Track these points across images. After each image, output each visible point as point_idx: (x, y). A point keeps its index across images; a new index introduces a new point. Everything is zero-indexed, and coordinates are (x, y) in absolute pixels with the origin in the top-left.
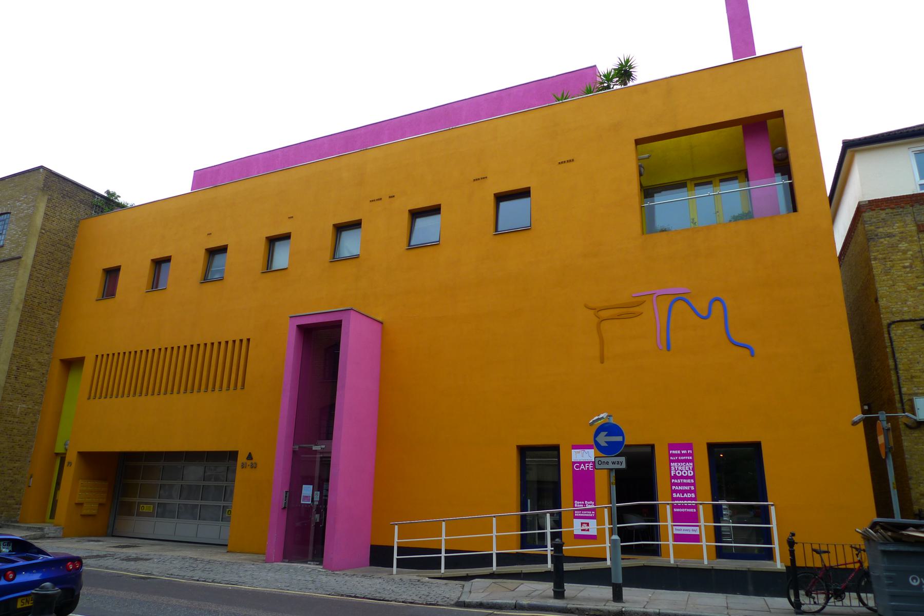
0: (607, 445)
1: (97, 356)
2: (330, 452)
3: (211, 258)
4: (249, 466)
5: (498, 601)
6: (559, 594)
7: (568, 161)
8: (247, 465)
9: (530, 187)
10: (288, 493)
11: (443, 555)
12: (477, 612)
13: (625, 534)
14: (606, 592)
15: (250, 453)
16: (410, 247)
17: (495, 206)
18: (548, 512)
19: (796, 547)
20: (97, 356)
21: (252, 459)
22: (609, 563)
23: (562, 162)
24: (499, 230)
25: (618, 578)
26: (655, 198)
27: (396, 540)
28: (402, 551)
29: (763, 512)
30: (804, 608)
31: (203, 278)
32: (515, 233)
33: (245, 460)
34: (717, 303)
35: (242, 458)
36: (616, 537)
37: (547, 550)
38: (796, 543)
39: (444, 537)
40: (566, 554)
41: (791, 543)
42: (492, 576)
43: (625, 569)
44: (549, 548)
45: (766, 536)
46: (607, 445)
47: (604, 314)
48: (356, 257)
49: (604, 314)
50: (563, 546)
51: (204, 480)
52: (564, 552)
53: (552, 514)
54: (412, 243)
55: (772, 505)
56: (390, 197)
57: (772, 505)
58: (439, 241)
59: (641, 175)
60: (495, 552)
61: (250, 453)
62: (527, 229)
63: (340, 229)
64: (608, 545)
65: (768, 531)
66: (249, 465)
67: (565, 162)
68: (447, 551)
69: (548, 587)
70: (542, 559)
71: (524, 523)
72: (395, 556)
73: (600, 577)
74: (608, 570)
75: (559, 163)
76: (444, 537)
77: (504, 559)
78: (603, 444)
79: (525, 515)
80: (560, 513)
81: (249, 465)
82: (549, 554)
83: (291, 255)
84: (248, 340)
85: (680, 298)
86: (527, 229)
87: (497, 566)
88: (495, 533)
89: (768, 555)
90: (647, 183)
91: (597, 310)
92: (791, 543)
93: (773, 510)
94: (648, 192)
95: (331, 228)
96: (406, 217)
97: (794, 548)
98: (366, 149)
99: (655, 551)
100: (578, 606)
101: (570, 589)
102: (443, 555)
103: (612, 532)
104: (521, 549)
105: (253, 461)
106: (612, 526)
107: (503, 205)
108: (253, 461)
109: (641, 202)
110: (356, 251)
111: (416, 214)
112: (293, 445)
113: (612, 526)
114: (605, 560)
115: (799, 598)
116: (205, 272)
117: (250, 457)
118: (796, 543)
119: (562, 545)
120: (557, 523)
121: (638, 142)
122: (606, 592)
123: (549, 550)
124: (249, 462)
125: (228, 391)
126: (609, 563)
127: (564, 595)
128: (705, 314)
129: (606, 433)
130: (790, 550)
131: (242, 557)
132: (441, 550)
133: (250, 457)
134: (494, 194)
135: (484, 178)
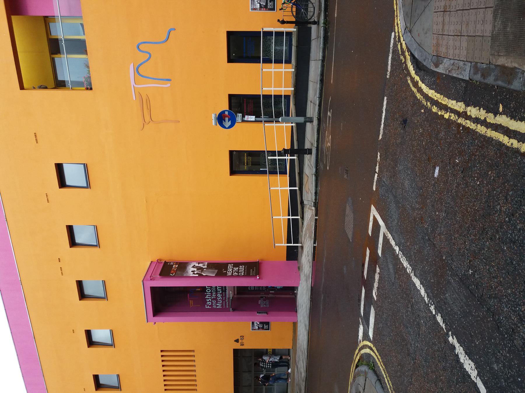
0: (230, 121)
1: (165, 390)
2: (234, 287)
3: (102, 386)
4: (243, 340)
5: (314, 179)
6: (310, 152)
7: (36, 137)
8: (242, 342)
9: (85, 330)
10: (258, 312)
11: (291, 217)
12: (333, 53)
13: (279, 114)
14: (307, 157)
15: (235, 341)
16: (98, 245)
17: (68, 187)
18: (267, 158)
19: (285, 20)
20: (165, 390)
21: (238, 339)
22: (293, 125)
23: (37, 141)
24: (111, 343)
25: (301, 120)
26: (59, 38)
27: (283, 245)
28: (289, 241)
29: (268, 34)
30: (316, 20)
31: (118, 389)
32: (120, 377)
33: (239, 344)
34: (141, 47)
35: (238, 346)
36: (280, 119)
37: (288, 159)
38: (283, 19)
39: (281, 217)
40: (289, 147)
41: (283, 22)
42: (301, 189)
43: (297, 115)
44: (286, 158)
45: (279, 34)
46: (230, 121)
47: (147, 119)
48: (112, 332)
49: (147, 119)
50: (285, 149)
51: (251, 386)
52: (289, 149)
53: (268, 156)
54: (95, 244)
55: (263, 29)
56: (59, 262)
57: (263, 29)
58: (94, 226)
59: (46, 88)
60: (289, 188)
61: (235, 341)
62: (86, 166)
63: (91, 343)
64: (284, 125)
65: (277, 33)
66: (242, 341)
67: (36, 139)
68: (289, 215)
69: (307, 157)
70: (292, 161)
71: (273, 172)
72: (292, 245)
73: (301, 129)
74: (298, 124)
75: (37, 143)
76: (281, 217)
77: (292, 183)
78: (230, 123)
79: (269, 171)
80: (268, 151)
81: (242, 341)
82: (289, 158)
83: (102, 328)
84: (162, 351)
85: (137, 70)
86: (96, 227)
87: (296, 187)
88: (279, 188)
89: (289, 34)
90: (52, 83)
91: (144, 123)
92: (283, 22)
93: (266, 29)
94: (60, 85)
95: (82, 302)
96: (75, 249)
97: (286, 21)
98: (21, 280)
99: (287, 97)
100: (316, 141)
101: (307, 146)
102: (291, 217)
103: (277, 122)
104: (287, 174)
105: (239, 338)
106: (274, 121)
107: (78, 240)
108: (239, 338)
109: (68, 89)
110: (108, 332)
111: (62, 184)
112: (230, 311)
113: (274, 121)
114: (292, 126)
115: (311, 22)
116: (115, 389)
117: (237, 341)
118: (283, 19)
119: (284, 149)
120: (273, 153)
121: (22, 87)
122: (308, 125)
123: (288, 158)
124: (240, 341)
125: (197, 385)
126: (293, 125)
127: (310, 149)
128: (148, 56)
129: (223, 121)
130: (287, 24)
131: (300, 240)
132: (288, 218)
133: (237, 341)
134: (70, 247)
135: (47, 195)
